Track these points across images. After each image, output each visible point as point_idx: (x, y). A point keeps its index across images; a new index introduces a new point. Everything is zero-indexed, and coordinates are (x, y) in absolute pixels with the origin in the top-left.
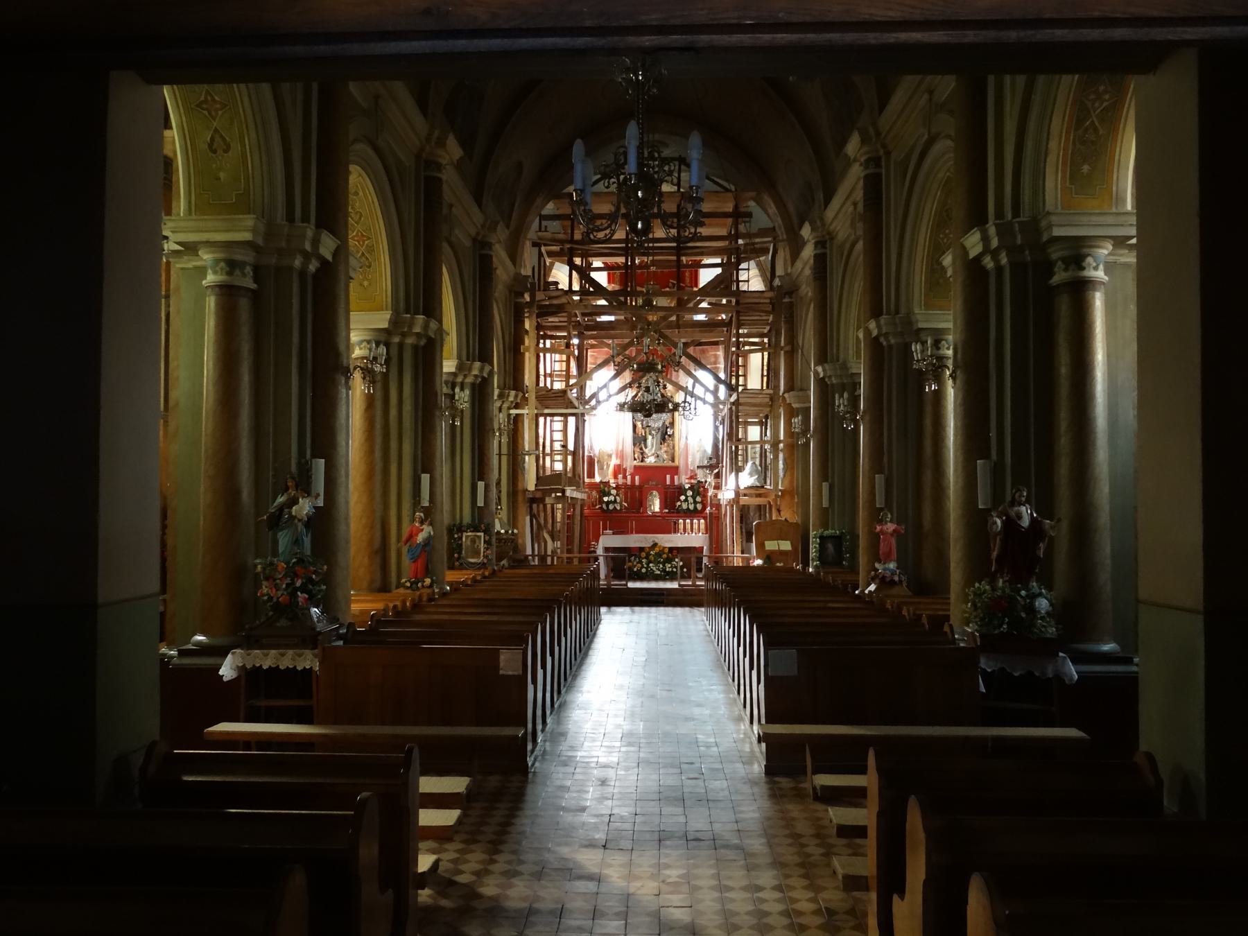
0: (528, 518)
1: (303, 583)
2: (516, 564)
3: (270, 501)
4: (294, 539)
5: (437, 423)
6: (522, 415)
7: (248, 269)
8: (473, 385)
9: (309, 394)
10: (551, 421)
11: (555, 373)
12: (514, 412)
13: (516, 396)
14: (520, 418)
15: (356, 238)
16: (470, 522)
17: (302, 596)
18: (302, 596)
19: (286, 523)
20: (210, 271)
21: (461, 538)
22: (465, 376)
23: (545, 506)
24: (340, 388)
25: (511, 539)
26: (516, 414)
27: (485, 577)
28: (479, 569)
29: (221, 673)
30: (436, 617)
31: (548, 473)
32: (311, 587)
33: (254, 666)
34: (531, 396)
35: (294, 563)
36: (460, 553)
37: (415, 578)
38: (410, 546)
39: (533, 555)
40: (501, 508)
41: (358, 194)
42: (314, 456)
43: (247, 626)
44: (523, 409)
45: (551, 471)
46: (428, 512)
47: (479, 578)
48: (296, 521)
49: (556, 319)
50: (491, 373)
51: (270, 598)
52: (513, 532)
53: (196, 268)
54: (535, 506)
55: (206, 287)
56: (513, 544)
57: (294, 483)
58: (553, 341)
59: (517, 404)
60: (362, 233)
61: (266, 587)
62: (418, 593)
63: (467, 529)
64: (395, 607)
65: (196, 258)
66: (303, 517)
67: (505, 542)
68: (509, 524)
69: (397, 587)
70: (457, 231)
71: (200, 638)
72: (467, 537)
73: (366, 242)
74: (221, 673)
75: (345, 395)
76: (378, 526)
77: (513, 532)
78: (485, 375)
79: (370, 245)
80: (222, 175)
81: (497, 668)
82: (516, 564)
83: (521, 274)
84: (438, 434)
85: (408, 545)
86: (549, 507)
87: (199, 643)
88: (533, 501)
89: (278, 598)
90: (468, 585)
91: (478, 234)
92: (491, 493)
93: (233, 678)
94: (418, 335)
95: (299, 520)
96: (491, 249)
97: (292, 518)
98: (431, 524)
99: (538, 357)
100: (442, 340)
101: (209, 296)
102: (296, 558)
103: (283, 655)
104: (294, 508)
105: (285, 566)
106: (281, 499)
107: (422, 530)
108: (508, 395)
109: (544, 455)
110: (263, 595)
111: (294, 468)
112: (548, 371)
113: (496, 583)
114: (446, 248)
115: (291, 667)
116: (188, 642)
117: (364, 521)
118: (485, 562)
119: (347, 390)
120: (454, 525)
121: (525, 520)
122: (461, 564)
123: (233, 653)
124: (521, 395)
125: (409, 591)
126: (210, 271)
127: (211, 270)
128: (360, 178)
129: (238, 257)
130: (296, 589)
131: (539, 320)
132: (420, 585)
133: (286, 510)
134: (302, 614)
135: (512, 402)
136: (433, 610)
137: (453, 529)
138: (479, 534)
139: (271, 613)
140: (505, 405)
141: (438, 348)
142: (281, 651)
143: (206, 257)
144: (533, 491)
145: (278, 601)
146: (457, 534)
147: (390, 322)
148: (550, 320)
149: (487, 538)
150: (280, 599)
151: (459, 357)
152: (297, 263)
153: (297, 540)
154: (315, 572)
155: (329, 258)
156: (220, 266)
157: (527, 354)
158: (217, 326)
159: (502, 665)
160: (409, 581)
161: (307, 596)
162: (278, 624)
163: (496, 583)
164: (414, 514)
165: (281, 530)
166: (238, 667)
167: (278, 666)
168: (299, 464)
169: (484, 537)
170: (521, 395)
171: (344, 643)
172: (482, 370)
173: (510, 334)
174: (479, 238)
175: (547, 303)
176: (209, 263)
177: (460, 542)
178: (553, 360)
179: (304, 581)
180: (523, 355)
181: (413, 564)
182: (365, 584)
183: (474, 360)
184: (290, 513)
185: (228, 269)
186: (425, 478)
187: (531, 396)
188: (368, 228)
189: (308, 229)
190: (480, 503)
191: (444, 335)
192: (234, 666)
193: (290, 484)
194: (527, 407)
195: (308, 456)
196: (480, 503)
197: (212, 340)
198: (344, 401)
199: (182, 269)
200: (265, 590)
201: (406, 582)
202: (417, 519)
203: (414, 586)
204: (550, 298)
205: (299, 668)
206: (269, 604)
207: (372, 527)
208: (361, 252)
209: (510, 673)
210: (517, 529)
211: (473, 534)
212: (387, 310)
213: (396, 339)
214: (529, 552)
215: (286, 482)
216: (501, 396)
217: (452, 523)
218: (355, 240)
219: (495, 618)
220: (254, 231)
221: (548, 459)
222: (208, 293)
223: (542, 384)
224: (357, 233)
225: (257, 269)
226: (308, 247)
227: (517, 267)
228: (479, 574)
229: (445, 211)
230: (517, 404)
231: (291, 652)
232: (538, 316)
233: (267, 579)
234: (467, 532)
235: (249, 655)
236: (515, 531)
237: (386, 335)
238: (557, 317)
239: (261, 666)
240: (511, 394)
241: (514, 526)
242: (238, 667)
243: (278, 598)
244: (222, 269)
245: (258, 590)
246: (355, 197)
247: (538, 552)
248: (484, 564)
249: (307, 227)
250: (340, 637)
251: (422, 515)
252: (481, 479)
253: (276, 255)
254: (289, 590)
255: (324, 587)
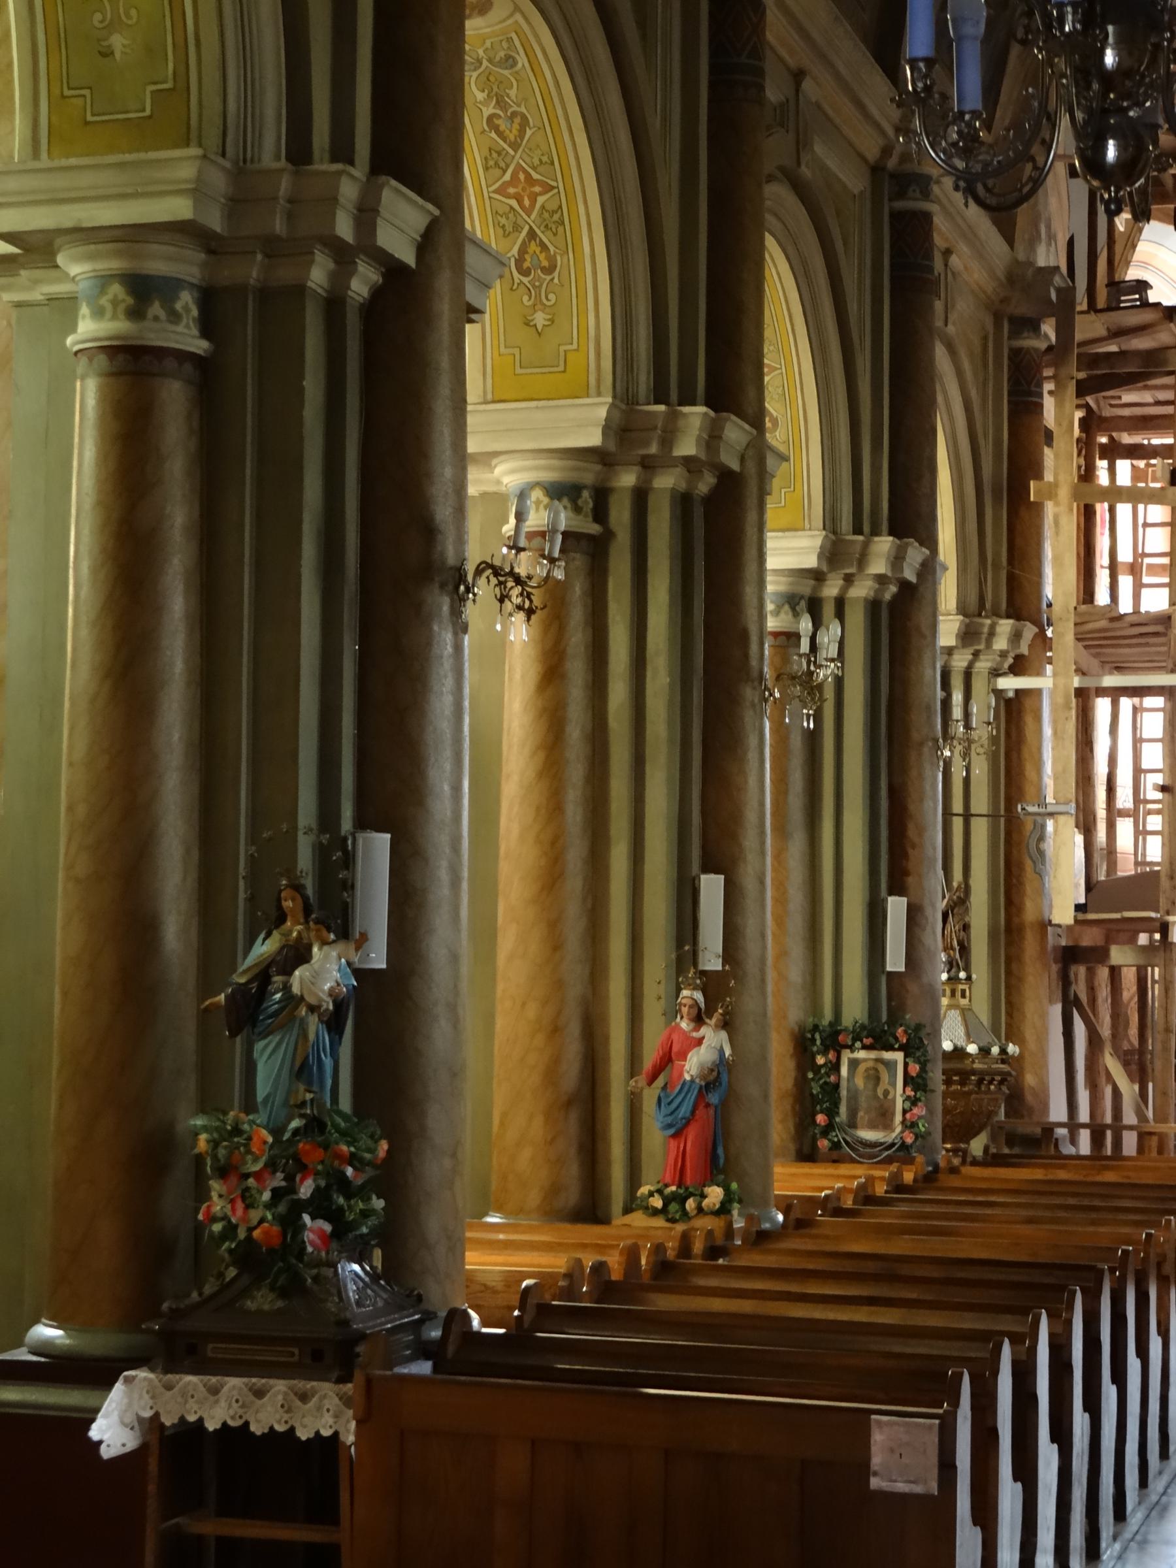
0: (1056, 1010)
1: (317, 1189)
2: (1017, 1150)
3: (239, 959)
4: (298, 1064)
5: (748, 716)
6: (1037, 693)
7: (186, 300)
8: (873, 606)
9: (350, 649)
10: (1136, 710)
11: (1147, 561)
12: (1008, 683)
13: (1016, 636)
14: (1028, 703)
15: (511, 190)
16: (866, 1022)
17: (314, 1227)
18: (314, 1227)
19: (276, 1014)
20: (84, 310)
21: (836, 1067)
22: (849, 580)
23: (1115, 972)
24: (436, 628)
25: (1000, 1073)
26: (1017, 691)
27: (898, 1187)
28: (889, 1161)
29: (94, 1433)
30: (717, 1305)
31: (1126, 868)
32: (341, 1200)
33: (182, 1419)
34: (1063, 634)
35: (296, 1132)
36: (832, 1112)
37: (679, 1186)
38: (664, 1088)
39: (1073, 1126)
40: (969, 978)
41: (515, 63)
42: (363, 823)
43: (165, 1306)
44: (1040, 673)
45: (1137, 864)
46: (713, 986)
47: (880, 1189)
48: (303, 1011)
49: (1147, 397)
50: (929, 569)
51: (230, 1230)
52: (1003, 1051)
53: (51, 300)
54: (1080, 971)
55: (76, 353)
56: (1004, 1089)
57: (299, 900)
58: (1141, 464)
59: (1019, 658)
60: (528, 175)
61: (220, 1196)
62: (680, 1228)
63: (854, 1040)
64: (599, 1268)
65: (53, 273)
66: (321, 1000)
67: (980, 1082)
68: (995, 1030)
69: (627, 1210)
70: (819, 148)
71: (47, 1332)
72: (854, 1063)
73: (541, 200)
74: (94, 1433)
75: (449, 649)
76: (574, 1029)
77: (1003, 1051)
78: (910, 575)
79: (550, 207)
80: (118, 42)
81: (864, 1469)
82: (1017, 1150)
83: (1030, 264)
84: (752, 756)
85: (660, 1081)
86: (1129, 977)
87: (41, 1348)
88: (1070, 956)
89: (250, 1230)
90: (839, 1212)
91: (887, 151)
92: (929, 929)
93: (128, 1449)
94: (688, 461)
95: (312, 1009)
96: (926, 194)
97: (292, 1001)
98: (726, 1025)
99: (1088, 514)
100: (763, 477)
101: (83, 379)
102: (302, 1116)
103: (259, 1393)
104: (297, 973)
105: (270, 1140)
106: (264, 948)
107: (699, 1042)
108: (992, 634)
109: (1113, 813)
110: (214, 1219)
111: (305, 859)
112: (1125, 555)
113: (928, 1209)
114: (778, 195)
115: (280, 1428)
116: (18, 1343)
117: (532, 1011)
118: (909, 1140)
119: (455, 634)
120: (816, 1028)
121: (1044, 1016)
122: (836, 1146)
123: (128, 1381)
124: (1030, 631)
125: (660, 1222)
126: (84, 310)
127: (88, 304)
128: (518, 17)
129: (157, 267)
130: (298, 1207)
131: (1090, 400)
132: (690, 1204)
133: (278, 979)
134: (316, 1279)
135: (1003, 654)
136: (713, 1282)
137: (813, 1040)
138: (888, 1055)
139: (232, 1272)
140: (983, 665)
141: (751, 502)
142: (254, 1380)
143: (75, 269)
144: (1069, 928)
145: (249, 1238)
146: (825, 1052)
147: (606, 429)
148: (1128, 397)
149: (914, 1068)
150: (256, 1234)
151: (831, 523)
152: (318, 275)
153: (304, 1065)
154: (352, 1159)
155: (408, 256)
156: (110, 296)
157: (1050, 509)
158: (103, 457)
159: (876, 1460)
160: (660, 1192)
161: (328, 1227)
162: (250, 1305)
163: (928, 1209)
164: (678, 990)
165: (264, 1035)
166: (140, 1420)
167: (247, 1424)
168: (322, 853)
169: (906, 1065)
170: (1030, 631)
171: (436, 1369)
172: (897, 559)
173: (998, 443)
174: (892, 163)
175: (1113, 348)
176: (83, 287)
177: (833, 1079)
178: (1141, 521)
179: (323, 1183)
180: (1038, 508)
181: (673, 1144)
182: (534, 1198)
183: (875, 532)
184: (286, 988)
185: (130, 301)
186: (712, 887)
187: (1063, 634)
188: (545, 159)
189: (344, 180)
190: (895, 961)
191: (770, 461)
192: (130, 1418)
193: (288, 904)
194: (1049, 668)
195: (347, 825)
196: (895, 961)
197: (89, 502)
198: (447, 665)
199: (19, 305)
200: (218, 1206)
201: (651, 1194)
202: (685, 1010)
203: (673, 1207)
204: (1117, 333)
205: (303, 1435)
206: (227, 1244)
207: (556, 1030)
208: (527, 228)
209: (901, 1487)
210: (1020, 1042)
211: (873, 1055)
212: (599, 394)
213: (627, 479)
214: (1058, 1112)
215: (279, 900)
216: (968, 636)
217: (810, 1021)
218: (509, 196)
219: (860, 1315)
220: (198, 192)
221: (1125, 828)
222: (80, 370)
223: (1102, 597)
224: (514, 175)
225: (208, 297)
226: (344, 229)
227: (1016, 244)
228: (882, 1178)
229: (773, 94)
230: (1019, 658)
231: (280, 1386)
232: (1083, 389)
233: (223, 1172)
234: (851, 1048)
235: (169, 1387)
236: (1012, 1049)
237: (599, 467)
238: (1146, 388)
239: (201, 1420)
240: (999, 629)
241: (1013, 1034)
242: (140, 1420)
243: (250, 1230)
244: (115, 303)
245: (202, 1202)
246: (506, 72)
247: (1092, 1115)
248: (904, 1146)
249: (339, 173)
250: (424, 1350)
251: (699, 996)
252: (897, 888)
253: (259, 257)
254: (282, 1208)
255: (378, 1204)
